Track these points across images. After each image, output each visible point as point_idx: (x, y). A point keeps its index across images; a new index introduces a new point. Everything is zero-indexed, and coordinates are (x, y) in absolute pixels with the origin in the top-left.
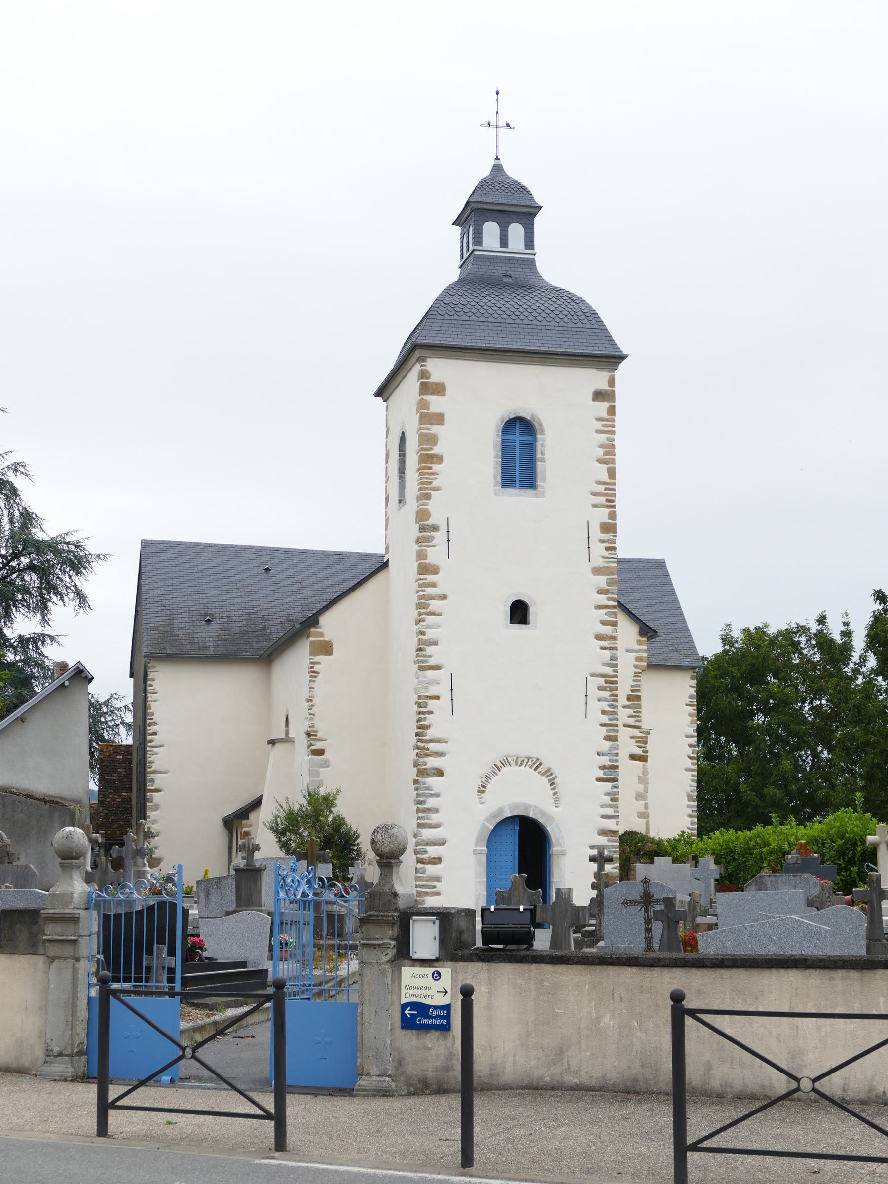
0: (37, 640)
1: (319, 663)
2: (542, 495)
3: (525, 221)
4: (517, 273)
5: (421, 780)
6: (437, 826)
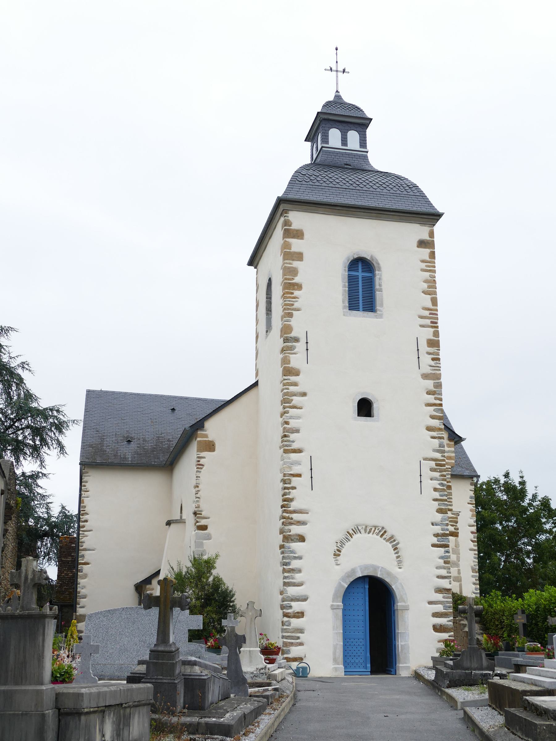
0: (35, 476)
1: (204, 458)
2: (381, 316)
3: (359, 129)
4: (355, 163)
5: (286, 544)
6: (300, 584)
